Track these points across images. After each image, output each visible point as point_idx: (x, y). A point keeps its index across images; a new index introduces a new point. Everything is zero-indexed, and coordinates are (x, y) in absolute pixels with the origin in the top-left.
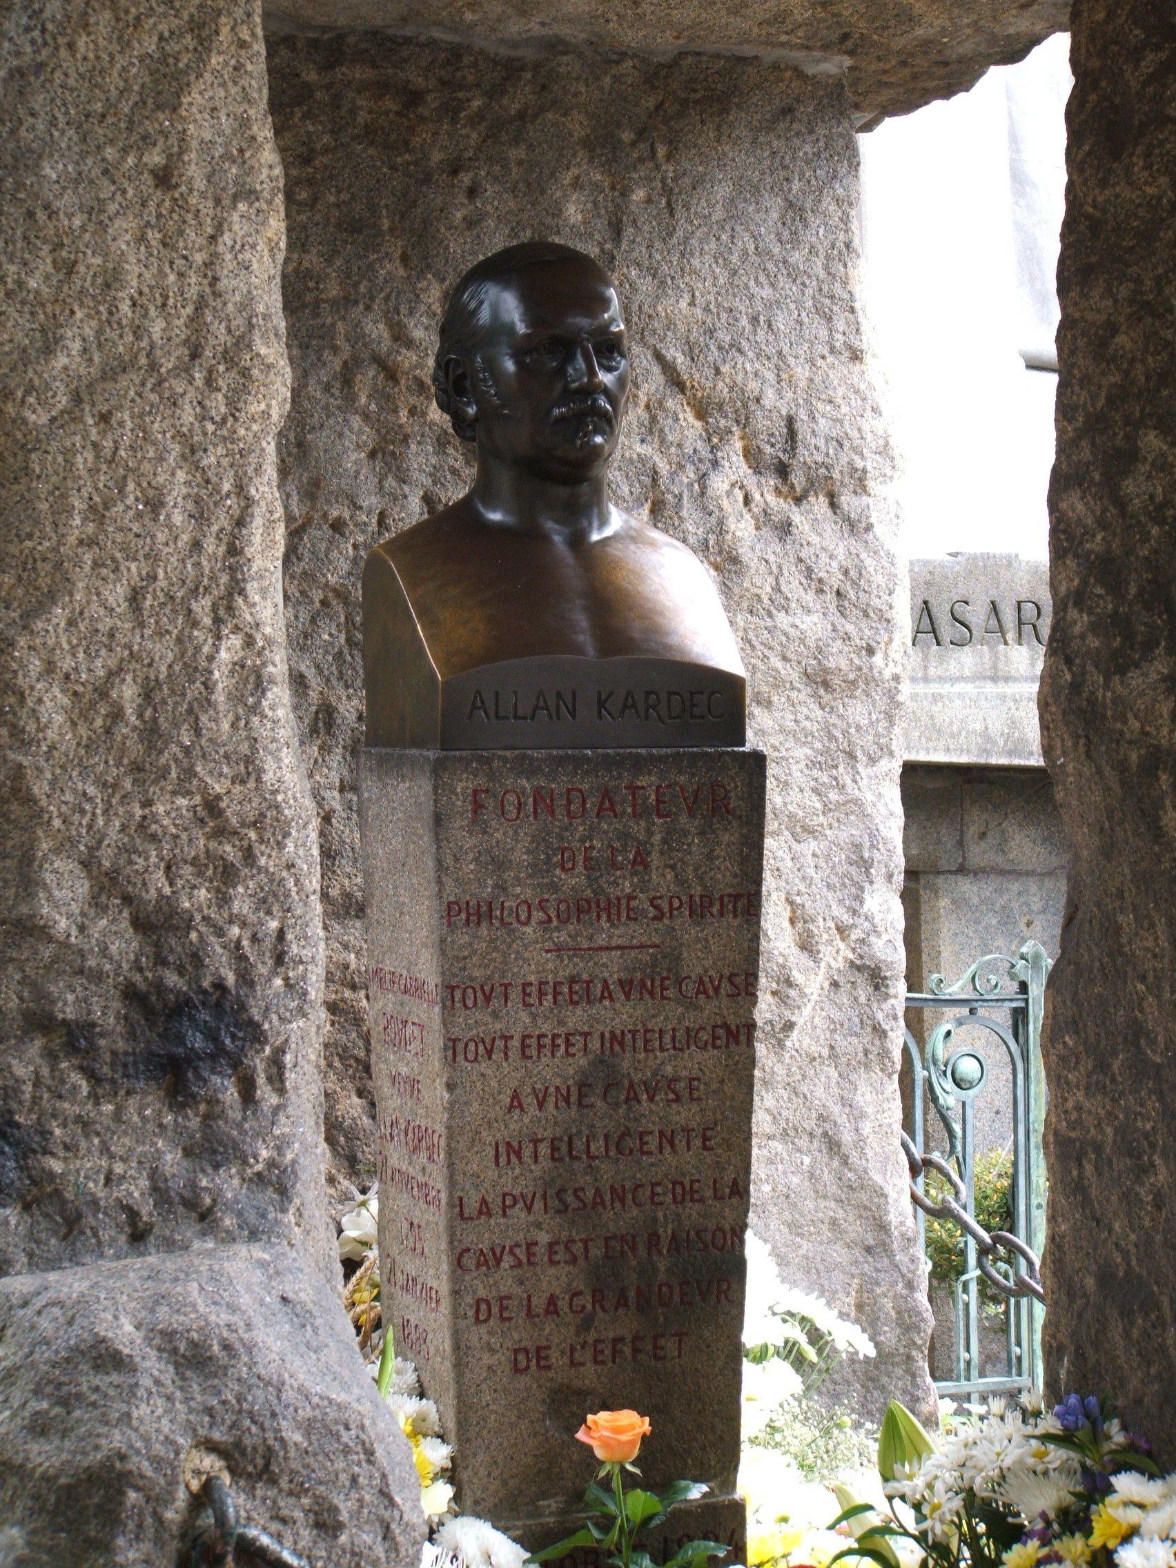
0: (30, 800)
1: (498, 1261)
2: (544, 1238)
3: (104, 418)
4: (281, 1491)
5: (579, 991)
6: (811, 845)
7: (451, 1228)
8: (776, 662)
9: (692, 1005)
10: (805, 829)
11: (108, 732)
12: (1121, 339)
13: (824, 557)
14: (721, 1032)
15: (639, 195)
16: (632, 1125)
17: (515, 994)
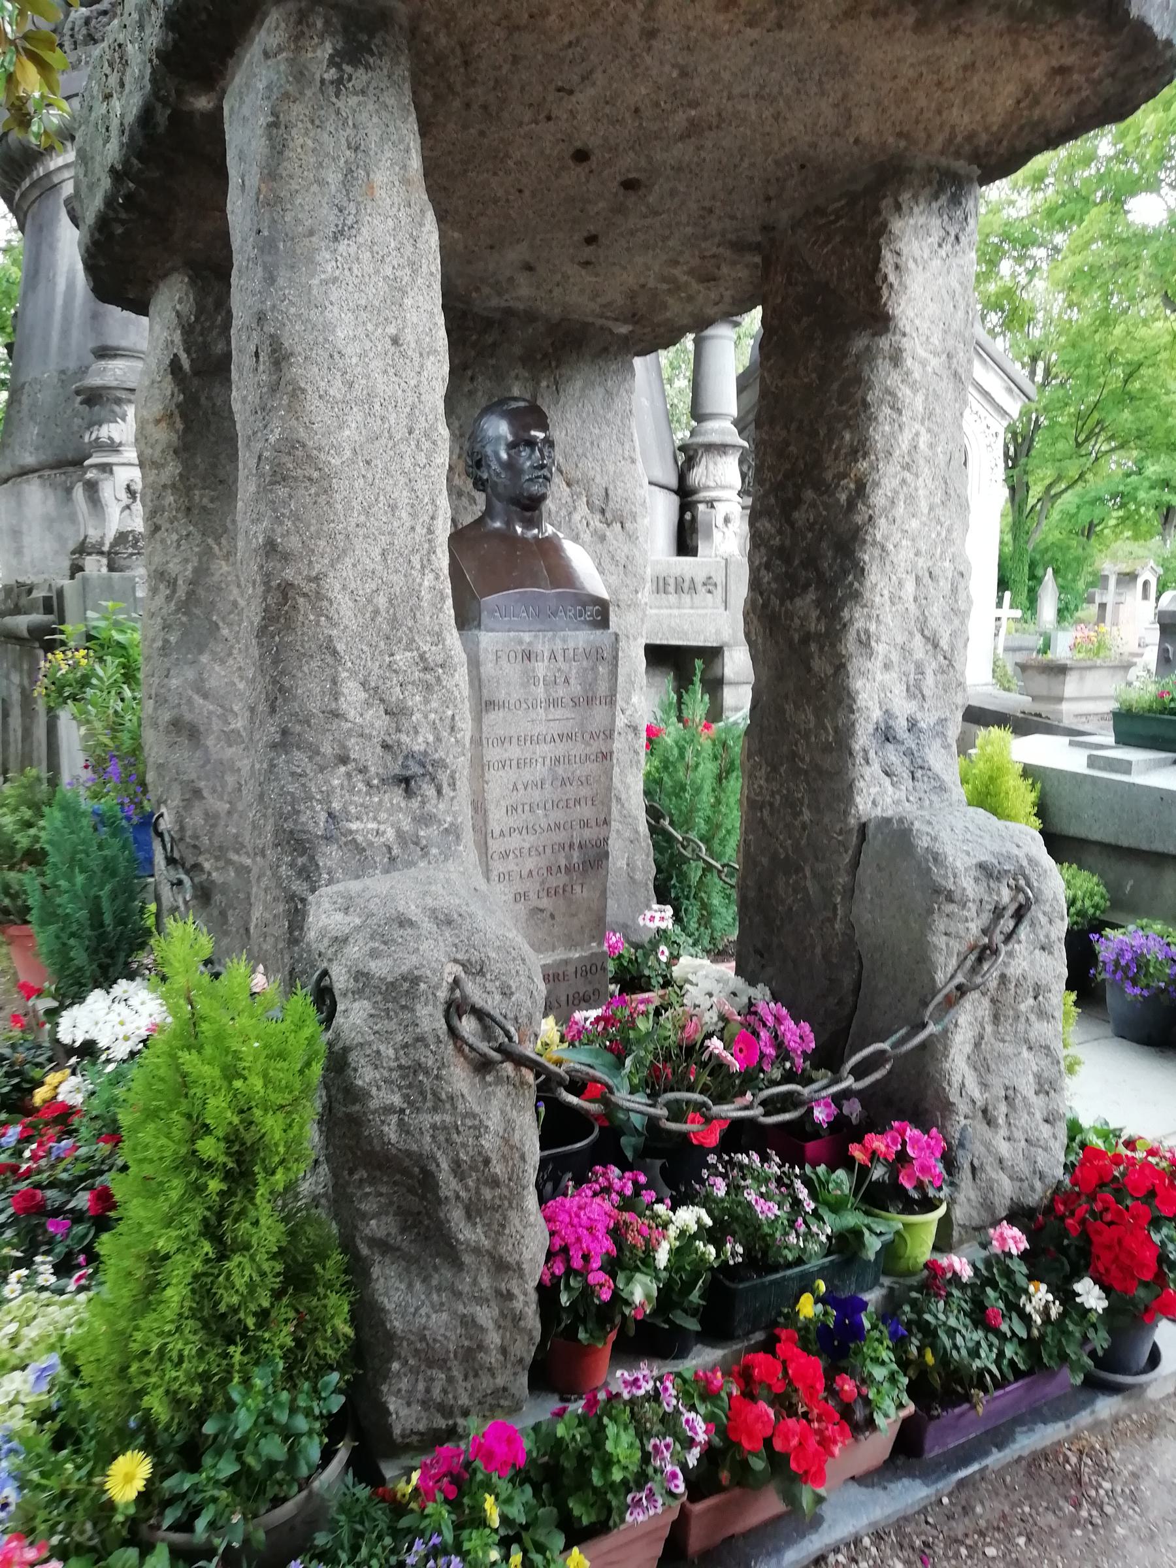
0: (335, 653)
2: (527, 845)
9: (588, 744)
12: (792, 448)
15: (544, 384)
17: (514, 740)
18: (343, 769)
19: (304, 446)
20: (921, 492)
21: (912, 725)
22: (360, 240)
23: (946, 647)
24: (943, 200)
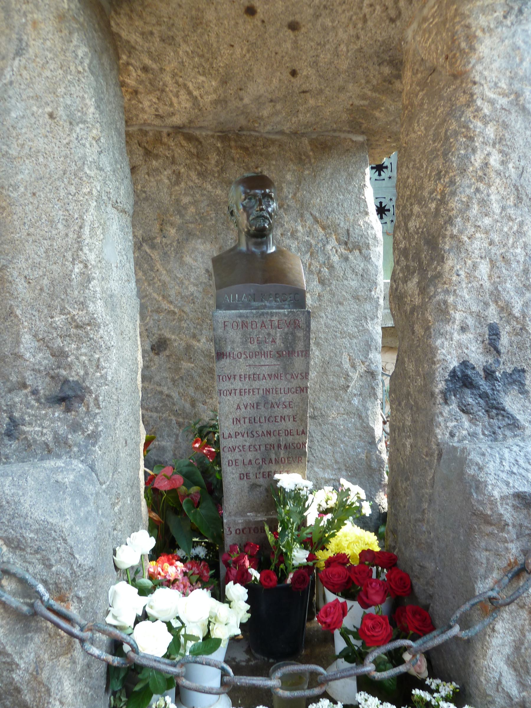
1: (234, 450)
2: (248, 444)
4: (27, 553)
5: (255, 377)
9: (289, 381)
10: (353, 336)
11: (40, 295)
13: (357, 266)
14: (299, 389)
16: (273, 414)
17: (237, 378)
20: (493, 197)
21: (489, 374)
23: (517, 315)
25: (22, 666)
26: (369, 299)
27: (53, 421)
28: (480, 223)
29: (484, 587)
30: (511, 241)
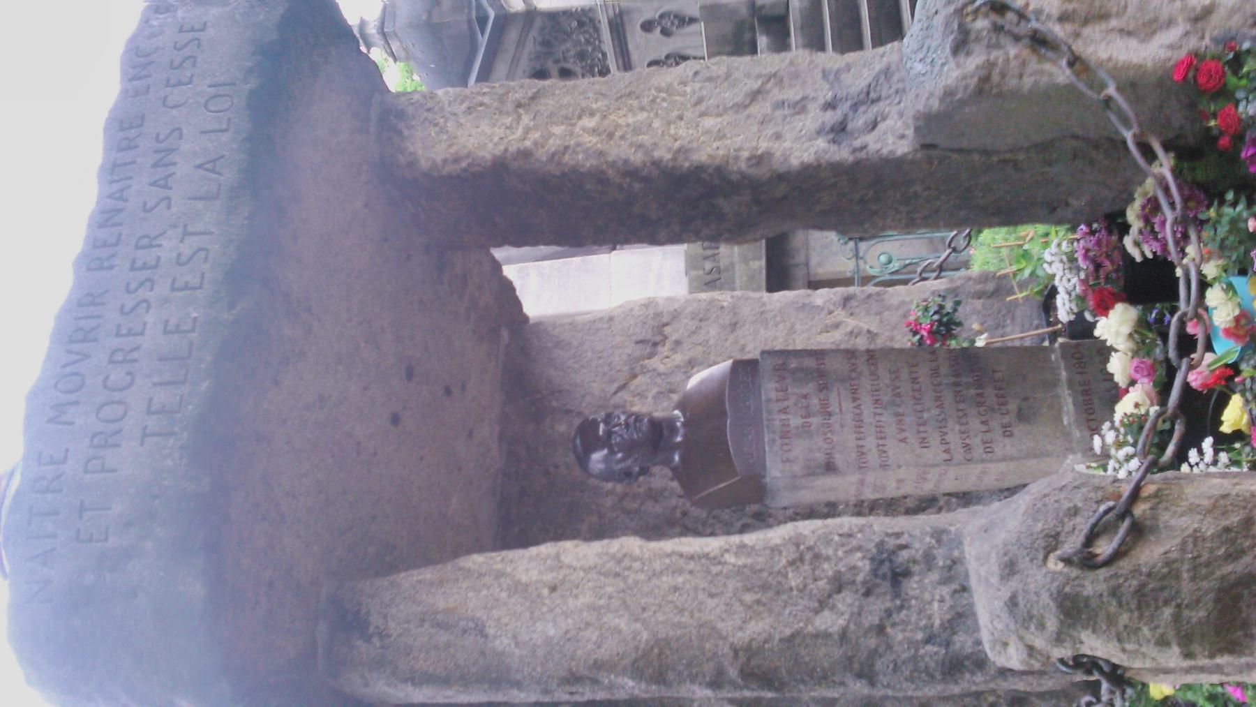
2: (957, 427)
3: (644, 609)
5: (859, 423)
6: (798, 326)
7: (958, 465)
8: (728, 343)
9: (861, 373)
15: (555, 404)
17: (861, 443)
18: (889, 630)
19: (635, 661)
20: (631, 120)
21: (830, 106)
22: (485, 617)
23: (759, 83)
24: (401, 126)
25: (1196, 526)
26: (734, 310)
27: (923, 589)
28: (660, 132)
29: (1061, 74)
30: (677, 98)
